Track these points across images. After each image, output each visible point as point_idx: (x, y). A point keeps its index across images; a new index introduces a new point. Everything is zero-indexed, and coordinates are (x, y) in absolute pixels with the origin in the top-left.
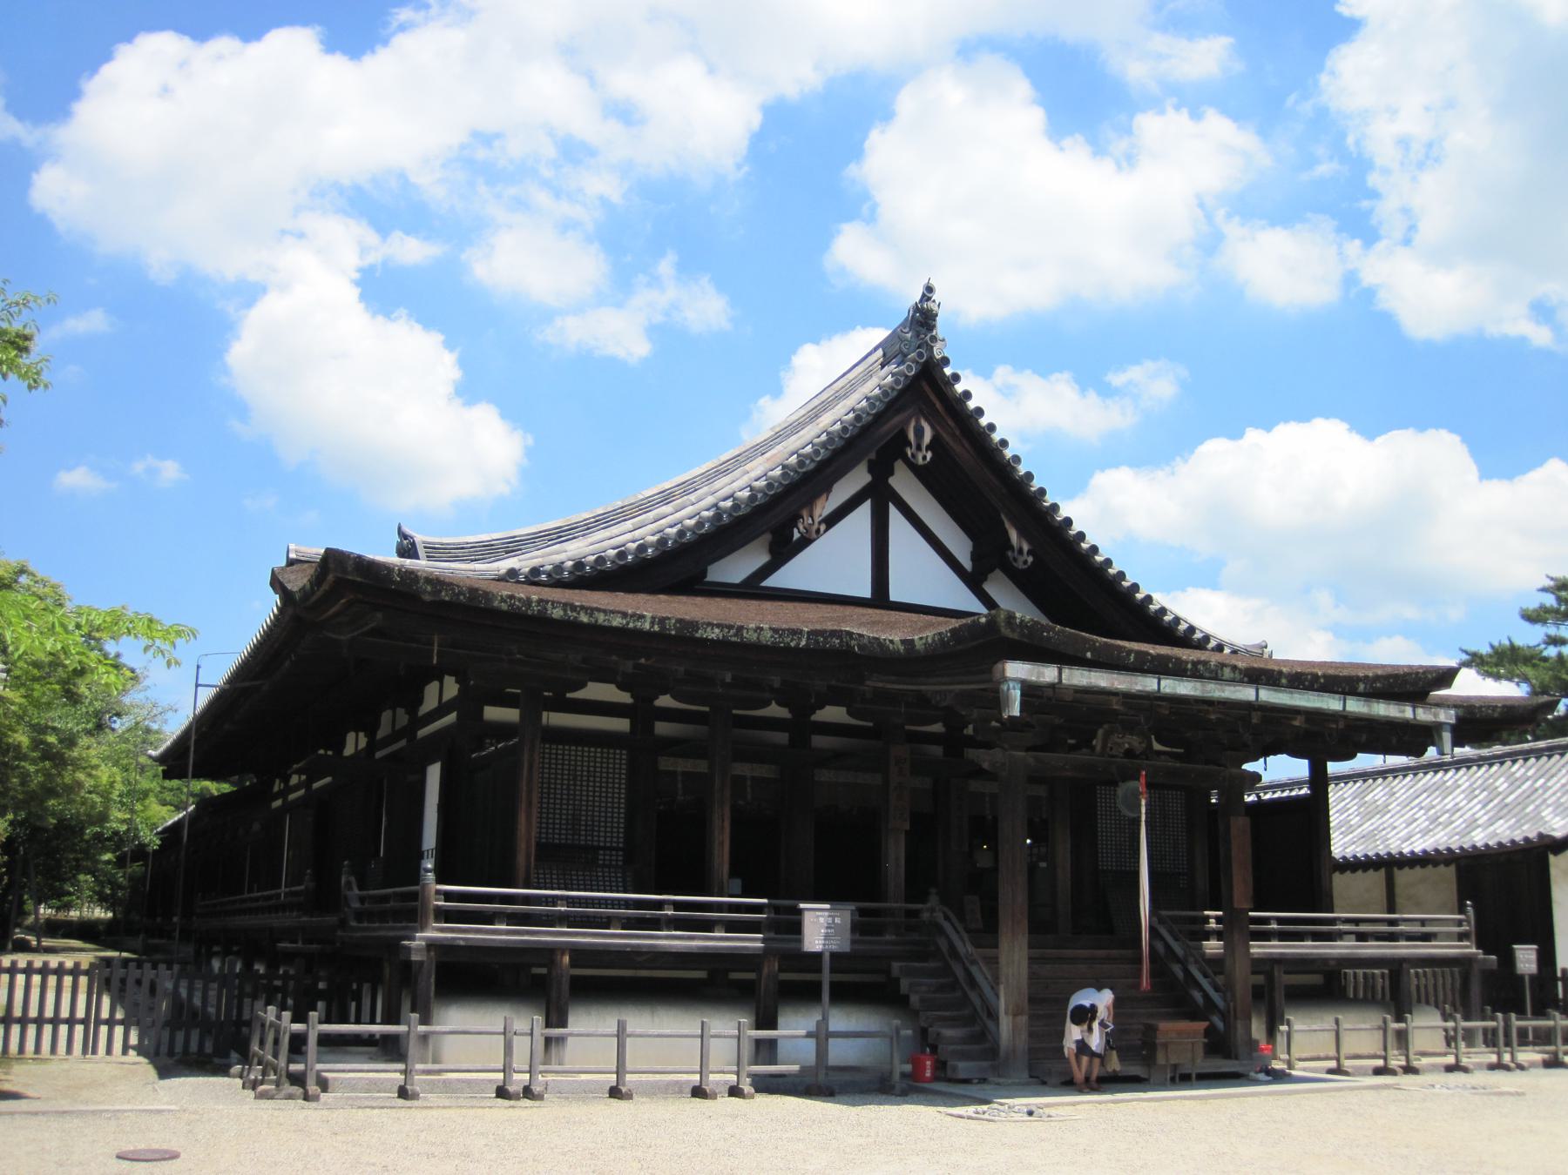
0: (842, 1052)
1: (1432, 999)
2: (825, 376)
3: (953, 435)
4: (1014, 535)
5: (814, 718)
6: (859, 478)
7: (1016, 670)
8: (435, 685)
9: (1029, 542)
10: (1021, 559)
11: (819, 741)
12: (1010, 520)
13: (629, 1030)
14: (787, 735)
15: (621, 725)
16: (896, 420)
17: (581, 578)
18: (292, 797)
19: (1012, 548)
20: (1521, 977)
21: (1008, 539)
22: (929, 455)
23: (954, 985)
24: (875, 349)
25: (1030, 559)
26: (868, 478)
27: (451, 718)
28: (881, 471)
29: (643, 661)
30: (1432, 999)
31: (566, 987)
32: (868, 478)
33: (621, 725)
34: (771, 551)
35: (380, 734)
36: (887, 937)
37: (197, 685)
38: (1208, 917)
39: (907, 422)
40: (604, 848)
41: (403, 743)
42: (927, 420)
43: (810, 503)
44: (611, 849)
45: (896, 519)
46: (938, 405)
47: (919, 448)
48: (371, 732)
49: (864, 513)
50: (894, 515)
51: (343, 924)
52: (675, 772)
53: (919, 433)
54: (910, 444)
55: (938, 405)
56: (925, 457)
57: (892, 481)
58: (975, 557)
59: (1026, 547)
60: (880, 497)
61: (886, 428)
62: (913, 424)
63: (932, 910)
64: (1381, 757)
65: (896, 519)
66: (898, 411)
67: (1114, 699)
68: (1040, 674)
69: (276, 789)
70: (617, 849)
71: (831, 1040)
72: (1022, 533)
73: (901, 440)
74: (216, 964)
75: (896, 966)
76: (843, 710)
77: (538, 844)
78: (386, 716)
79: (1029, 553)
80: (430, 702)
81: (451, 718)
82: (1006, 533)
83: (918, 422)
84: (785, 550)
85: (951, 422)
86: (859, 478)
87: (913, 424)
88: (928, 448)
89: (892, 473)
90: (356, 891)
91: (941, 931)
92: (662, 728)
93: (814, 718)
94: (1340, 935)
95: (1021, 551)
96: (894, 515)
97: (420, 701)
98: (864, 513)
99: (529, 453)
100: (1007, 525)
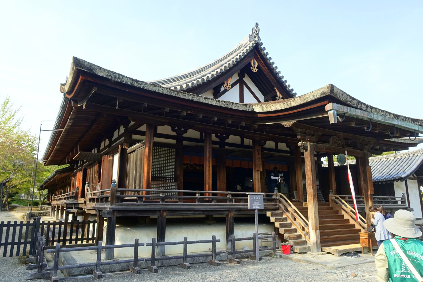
2: (230, 46)
4: (278, 93)
5: (226, 141)
6: (236, 77)
9: (282, 95)
11: (185, 143)
15: (173, 141)
19: (278, 96)
22: (257, 70)
26: (238, 78)
28: (241, 76)
29: (189, 112)
31: (208, 214)
32: (238, 78)
33: (173, 141)
34: (214, 95)
35: (101, 148)
37: (41, 130)
38: (346, 197)
39: (251, 60)
40: (169, 178)
43: (227, 79)
44: (171, 178)
46: (259, 57)
47: (254, 68)
48: (98, 149)
49: (238, 85)
50: (245, 87)
51: (85, 202)
53: (254, 63)
54: (252, 66)
55: (259, 57)
56: (255, 70)
57: (244, 79)
59: (281, 97)
60: (241, 83)
63: (276, 195)
64: (376, 118)
66: (249, 57)
68: (361, 113)
70: (172, 178)
73: (249, 65)
77: (152, 177)
78: (103, 143)
80: (102, 147)
82: (276, 92)
84: (217, 94)
85: (262, 62)
86: (236, 77)
87: (253, 61)
88: (256, 68)
90: (89, 192)
91: (280, 202)
92: (185, 143)
93: (226, 141)
94: (388, 202)
96: (245, 87)
97: (112, 136)
98: (238, 85)
100: (276, 90)
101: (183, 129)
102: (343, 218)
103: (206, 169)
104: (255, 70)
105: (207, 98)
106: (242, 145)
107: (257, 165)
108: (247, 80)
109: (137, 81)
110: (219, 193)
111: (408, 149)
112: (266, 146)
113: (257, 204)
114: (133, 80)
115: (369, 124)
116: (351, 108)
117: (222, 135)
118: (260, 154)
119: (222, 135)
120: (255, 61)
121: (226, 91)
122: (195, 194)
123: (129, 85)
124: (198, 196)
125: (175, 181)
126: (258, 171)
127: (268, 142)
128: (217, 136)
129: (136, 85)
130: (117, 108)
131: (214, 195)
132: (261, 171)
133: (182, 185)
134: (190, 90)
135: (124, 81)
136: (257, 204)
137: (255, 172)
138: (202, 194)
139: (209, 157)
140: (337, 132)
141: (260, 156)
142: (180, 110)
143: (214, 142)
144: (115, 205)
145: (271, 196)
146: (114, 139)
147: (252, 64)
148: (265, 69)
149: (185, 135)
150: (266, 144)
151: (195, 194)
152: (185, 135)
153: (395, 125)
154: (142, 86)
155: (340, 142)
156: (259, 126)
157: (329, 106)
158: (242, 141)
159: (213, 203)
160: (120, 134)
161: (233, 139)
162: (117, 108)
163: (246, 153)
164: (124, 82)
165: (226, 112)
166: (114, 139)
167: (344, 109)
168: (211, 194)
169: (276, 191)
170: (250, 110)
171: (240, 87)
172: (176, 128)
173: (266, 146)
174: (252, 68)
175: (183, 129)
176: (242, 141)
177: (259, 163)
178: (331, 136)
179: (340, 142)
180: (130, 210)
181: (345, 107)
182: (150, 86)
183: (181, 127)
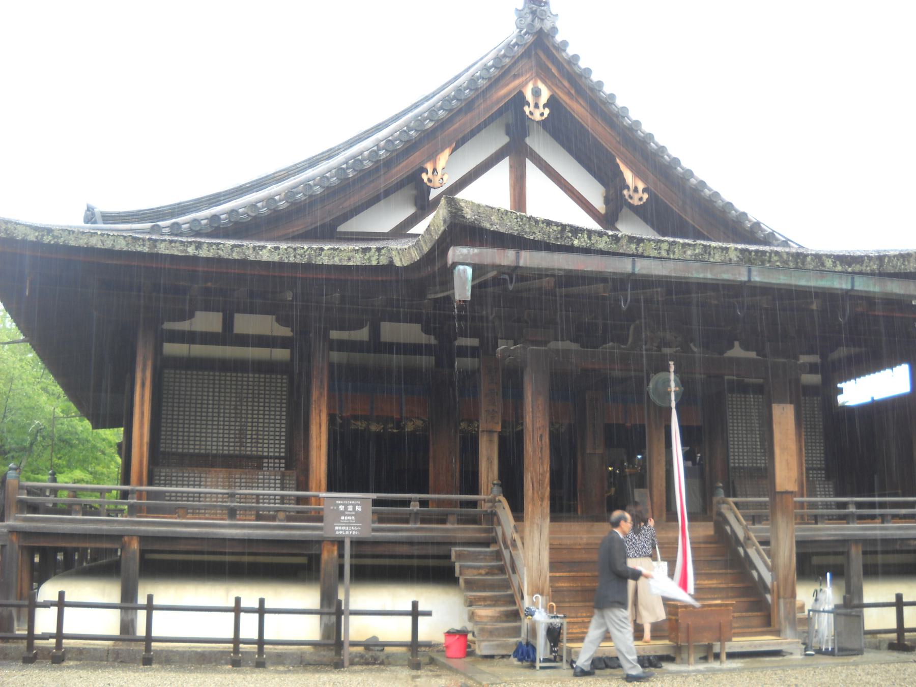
0: (431, 630)
3: (569, 94)
4: (628, 176)
10: (636, 197)
12: (622, 160)
13: (905, 600)
15: (281, 354)
16: (517, 82)
17: (218, 228)
19: (628, 188)
20: (663, 559)
21: (624, 180)
22: (547, 112)
23: (502, 570)
25: (646, 196)
32: (505, 140)
33: (281, 354)
40: (268, 457)
42: (544, 82)
44: (276, 458)
45: (533, 173)
46: (554, 70)
47: (537, 106)
53: (537, 93)
55: (554, 70)
58: (607, 200)
59: (641, 186)
61: (503, 92)
62: (530, 86)
64: (637, 270)
65: (533, 173)
67: (601, 286)
70: (280, 458)
72: (638, 173)
73: (519, 100)
75: (454, 550)
76: (417, 327)
79: (644, 190)
82: (622, 173)
83: (535, 83)
87: (530, 86)
88: (545, 106)
95: (636, 190)
100: (623, 167)
108: (539, 143)
109: (49, 231)
110: (433, 500)
113: (348, 524)
114: (36, 229)
120: (541, 85)
123: (32, 242)
124: (415, 507)
129: (47, 239)
131: (151, 495)
135: (19, 235)
136: (348, 524)
138: (424, 503)
144: (16, 519)
145: (474, 504)
147: (529, 96)
148: (578, 109)
151: (406, 503)
154: (62, 239)
157: (456, 253)
164: (20, 238)
167: (507, 257)
168: (144, 495)
170: (384, 261)
171: (511, 167)
174: (527, 109)
180: (45, 531)
182: (80, 236)
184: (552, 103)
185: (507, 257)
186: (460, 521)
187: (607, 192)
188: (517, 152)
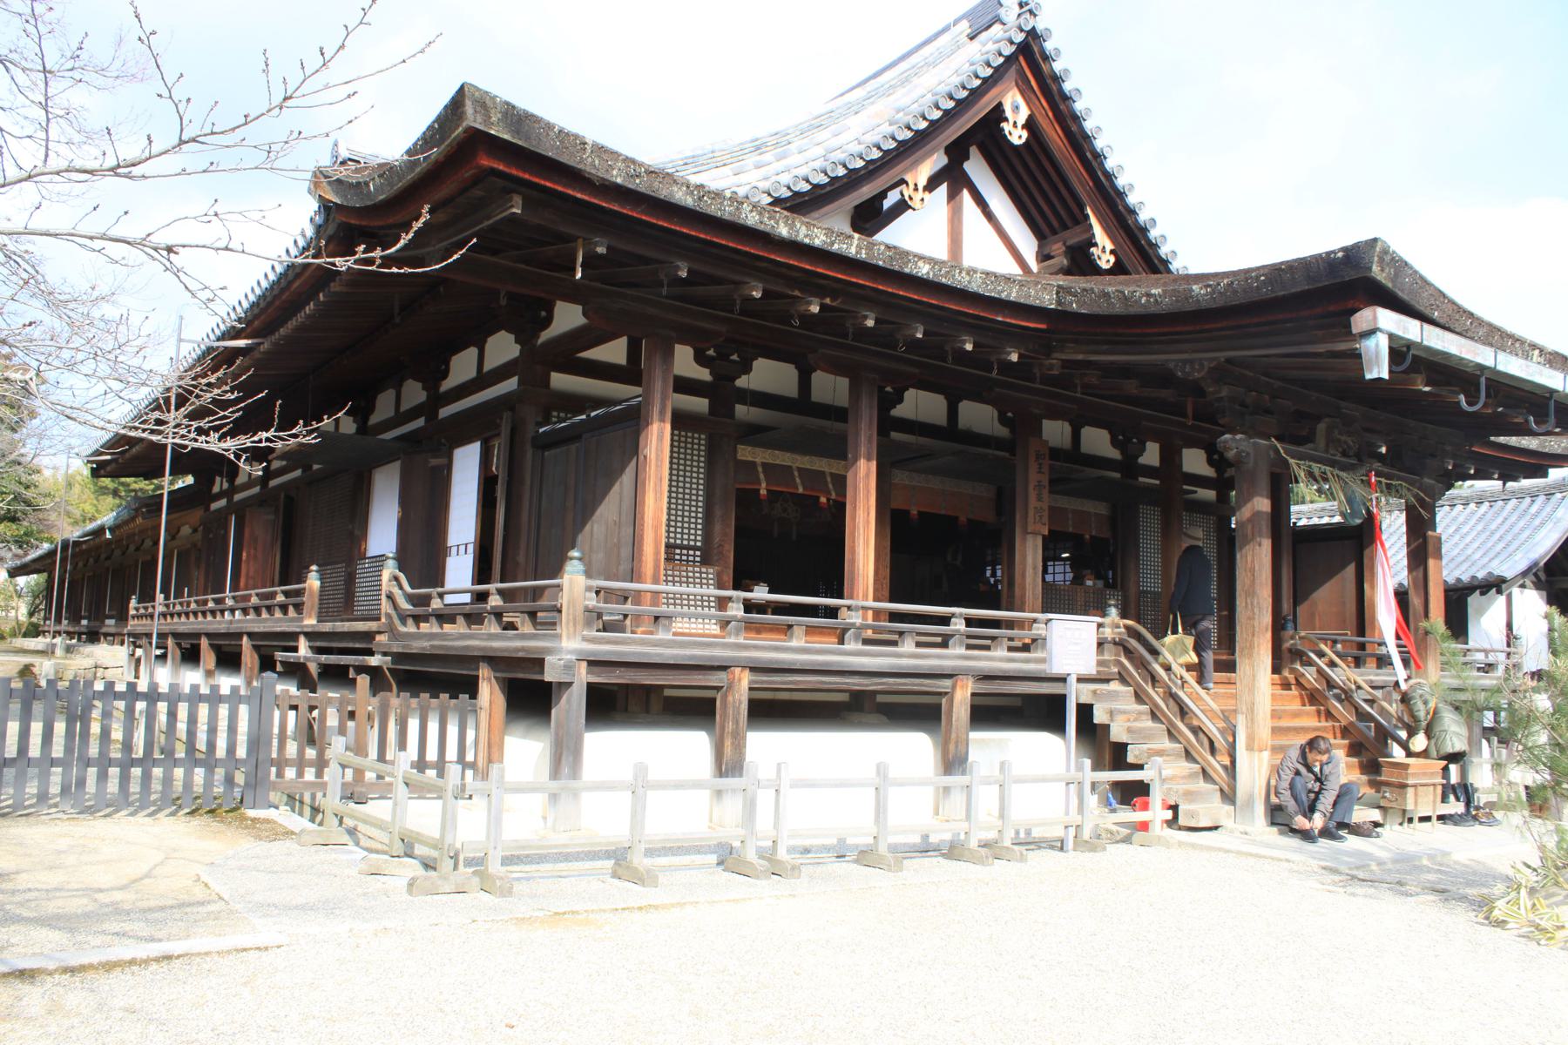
1: (1069, 223)
7: (1388, 320)
8: (472, 352)
14: (706, 401)
18: (237, 497)
19: (1096, 245)
24: (956, 22)
26: (944, 161)
27: (511, 384)
28: (957, 153)
30: (1069, 223)
32: (944, 161)
36: (794, 643)
40: (682, 547)
41: (420, 422)
44: (688, 548)
49: (943, 189)
52: (754, 463)
53: (1016, 108)
56: (1017, 136)
57: (967, 166)
64: (1500, 368)
68: (1405, 329)
69: (216, 489)
70: (695, 548)
71: (651, 794)
73: (997, 114)
74: (1089, 583)
79: (1112, 252)
81: (511, 384)
84: (870, 217)
89: (967, 158)
95: (1104, 250)
97: (445, 374)
99: (1181, 466)
100: (1093, 220)
101: (735, 357)
102: (542, 672)
103: (854, 518)
104: (1017, 136)
105: (827, 232)
106: (802, 404)
107: (1031, 513)
108: (977, 168)
110: (525, 589)
111: (1545, 475)
112: (899, 411)
115: (1547, 406)
116: (1426, 326)
117: (723, 356)
118: (1046, 469)
119: (723, 356)
121: (902, 206)
122: (945, 620)
125: (705, 561)
126: (1034, 533)
127: (910, 394)
128: (700, 359)
130: (579, 275)
132: (1044, 537)
133: (728, 576)
134: (802, 203)
137: (1024, 540)
139: (867, 475)
140: (1343, 404)
141: (1045, 480)
142: (797, 293)
143: (684, 385)
146: (447, 385)
147: (1008, 113)
148: (1053, 135)
149: (742, 382)
150: (901, 400)
151: (945, 620)
152: (742, 382)
153: (1552, 392)
155: (1349, 440)
156: (1067, 364)
158: (953, 412)
159: (794, 643)
160: (487, 367)
161: (769, 375)
162: (579, 275)
163: (993, 464)
165: (899, 288)
166: (447, 385)
167: (1411, 329)
169: (1113, 611)
172: (711, 352)
173: (899, 411)
174: (1004, 125)
175: (735, 357)
176: (953, 412)
177: (1039, 504)
178: (1319, 419)
179: (1349, 440)
181: (1417, 323)
183: (728, 354)
184: (1030, 125)
185: (1411, 329)
186: (919, 644)
187: (1040, 246)
188: (953, 178)
